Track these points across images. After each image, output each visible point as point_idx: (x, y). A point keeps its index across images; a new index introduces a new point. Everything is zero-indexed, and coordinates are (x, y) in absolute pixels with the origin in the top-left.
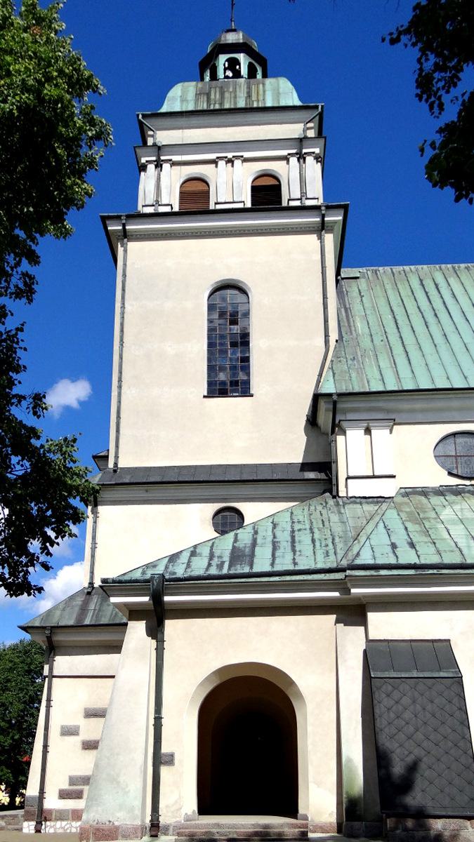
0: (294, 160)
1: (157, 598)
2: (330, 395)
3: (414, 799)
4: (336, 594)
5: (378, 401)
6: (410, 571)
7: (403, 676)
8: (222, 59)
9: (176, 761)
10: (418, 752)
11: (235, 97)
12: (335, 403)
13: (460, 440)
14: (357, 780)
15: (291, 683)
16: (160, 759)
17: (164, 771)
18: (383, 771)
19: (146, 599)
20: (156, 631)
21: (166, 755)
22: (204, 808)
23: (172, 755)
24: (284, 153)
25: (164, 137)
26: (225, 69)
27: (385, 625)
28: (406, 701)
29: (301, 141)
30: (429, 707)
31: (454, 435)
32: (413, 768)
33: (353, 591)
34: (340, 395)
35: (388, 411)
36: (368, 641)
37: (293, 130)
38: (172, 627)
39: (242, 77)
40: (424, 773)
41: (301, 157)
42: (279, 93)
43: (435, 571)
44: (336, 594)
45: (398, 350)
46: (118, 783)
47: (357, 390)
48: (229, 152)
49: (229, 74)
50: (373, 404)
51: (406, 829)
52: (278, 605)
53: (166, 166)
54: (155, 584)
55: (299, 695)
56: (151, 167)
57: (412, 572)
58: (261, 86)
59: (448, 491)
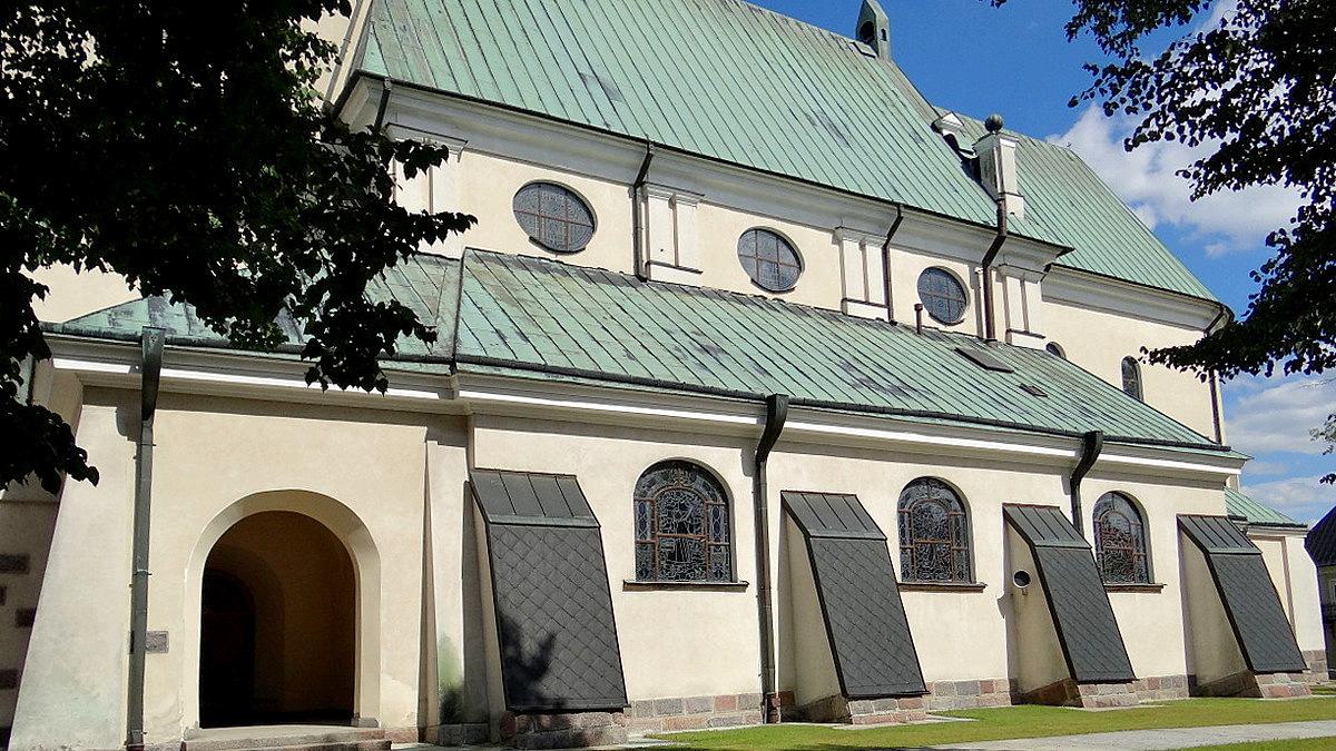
1: (150, 370)
2: (381, 79)
3: (550, 687)
4: (434, 396)
5: (448, 107)
6: (539, 373)
7: (530, 522)
9: (171, 646)
10: (550, 626)
12: (386, 94)
13: (545, 193)
14: (455, 666)
15: (355, 523)
16: (140, 643)
17: (151, 660)
18: (510, 651)
19: (125, 369)
20: (137, 425)
21: (155, 635)
22: (210, 717)
23: (164, 636)
27: (499, 449)
28: (532, 557)
30: (563, 566)
31: (539, 184)
32: (547, 645)
33: (463, 394)
34: (396, 83)
36: (471, 469)
38: (165, 421)
40: (560, 656)
43: (571, 379)
44: (434, 396)
45: (465, 34)
46: (77, 682)
47: (418, 82)
50: (438, 110)
51: (542, 729)
52: (261, 396)
54: (152, 345)
55: (369, 544)
57: (542, 376)
59: (514, 262)
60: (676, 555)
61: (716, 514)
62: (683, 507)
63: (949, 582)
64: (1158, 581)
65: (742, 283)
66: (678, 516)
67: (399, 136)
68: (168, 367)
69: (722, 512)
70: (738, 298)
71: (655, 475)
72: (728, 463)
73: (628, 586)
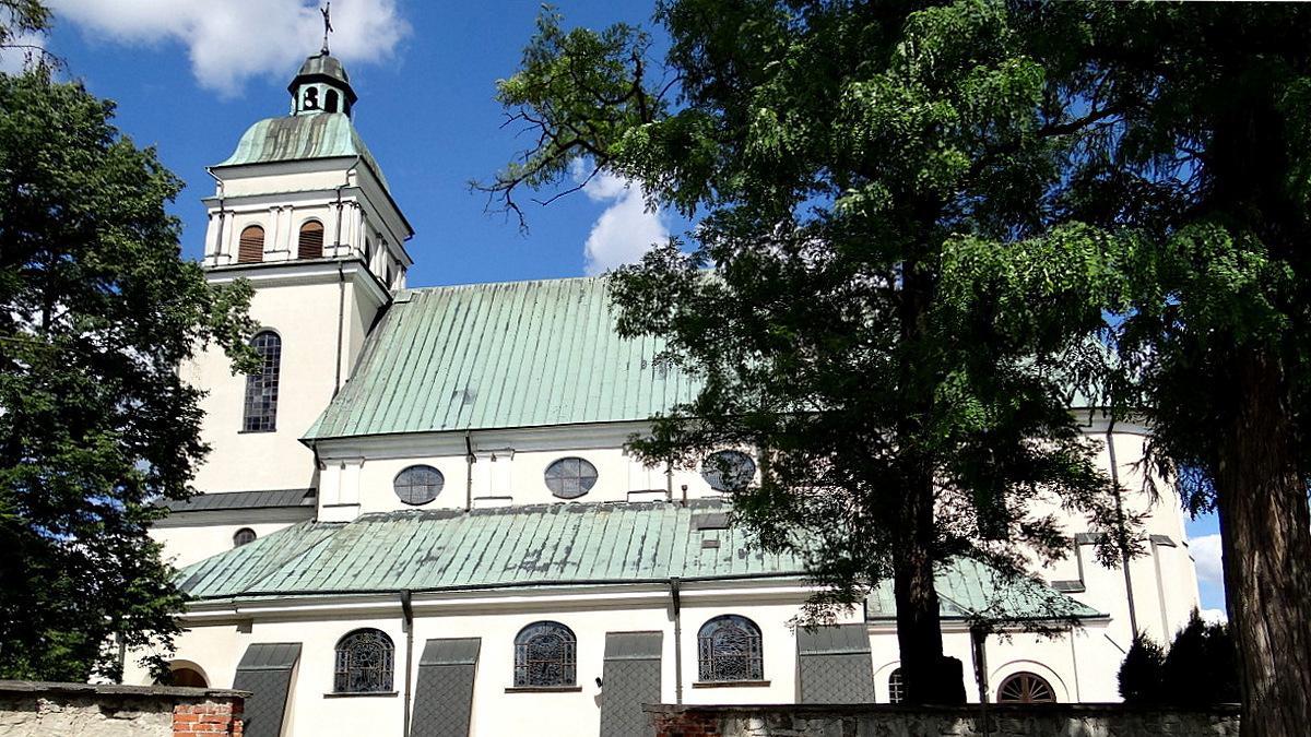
0: (334, 207)
8: (303, 89)
11: (298, 140)
24: (326, 201)
25: (232, 187)
26: (306, 99)
29: (339, 192)
31: (412, 468)
35: (360, 450)
37: (334, 178)
39: (319, 108)
41: (340, 205)
42: (336, 135)
48: (279, 201)
49: (309, 104)
50: (346, 446)
53: (228, 217)
56: (216, 218)
58: (323, 126)
60: (362, 679)
61: (754, 642)
62: (368, 654)
63: (559, 686)
64: (766, 678)
65: (548, 498)
66: (364, 658)
67: (148, 470)
68: (397, 608)
69: (758, 640)
70: (541, 509)
71: (715, 626)
72: (393, 627)
73: (696, 686)
